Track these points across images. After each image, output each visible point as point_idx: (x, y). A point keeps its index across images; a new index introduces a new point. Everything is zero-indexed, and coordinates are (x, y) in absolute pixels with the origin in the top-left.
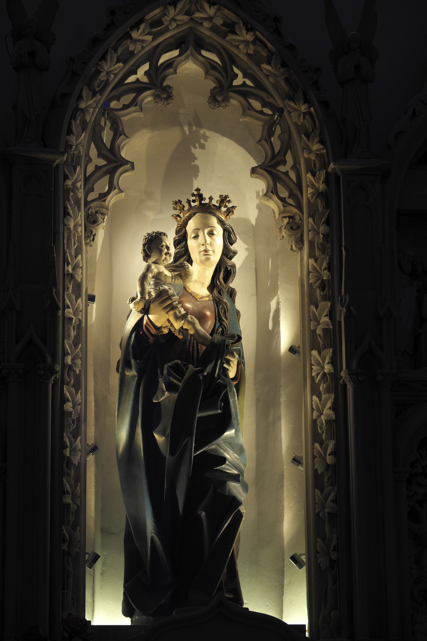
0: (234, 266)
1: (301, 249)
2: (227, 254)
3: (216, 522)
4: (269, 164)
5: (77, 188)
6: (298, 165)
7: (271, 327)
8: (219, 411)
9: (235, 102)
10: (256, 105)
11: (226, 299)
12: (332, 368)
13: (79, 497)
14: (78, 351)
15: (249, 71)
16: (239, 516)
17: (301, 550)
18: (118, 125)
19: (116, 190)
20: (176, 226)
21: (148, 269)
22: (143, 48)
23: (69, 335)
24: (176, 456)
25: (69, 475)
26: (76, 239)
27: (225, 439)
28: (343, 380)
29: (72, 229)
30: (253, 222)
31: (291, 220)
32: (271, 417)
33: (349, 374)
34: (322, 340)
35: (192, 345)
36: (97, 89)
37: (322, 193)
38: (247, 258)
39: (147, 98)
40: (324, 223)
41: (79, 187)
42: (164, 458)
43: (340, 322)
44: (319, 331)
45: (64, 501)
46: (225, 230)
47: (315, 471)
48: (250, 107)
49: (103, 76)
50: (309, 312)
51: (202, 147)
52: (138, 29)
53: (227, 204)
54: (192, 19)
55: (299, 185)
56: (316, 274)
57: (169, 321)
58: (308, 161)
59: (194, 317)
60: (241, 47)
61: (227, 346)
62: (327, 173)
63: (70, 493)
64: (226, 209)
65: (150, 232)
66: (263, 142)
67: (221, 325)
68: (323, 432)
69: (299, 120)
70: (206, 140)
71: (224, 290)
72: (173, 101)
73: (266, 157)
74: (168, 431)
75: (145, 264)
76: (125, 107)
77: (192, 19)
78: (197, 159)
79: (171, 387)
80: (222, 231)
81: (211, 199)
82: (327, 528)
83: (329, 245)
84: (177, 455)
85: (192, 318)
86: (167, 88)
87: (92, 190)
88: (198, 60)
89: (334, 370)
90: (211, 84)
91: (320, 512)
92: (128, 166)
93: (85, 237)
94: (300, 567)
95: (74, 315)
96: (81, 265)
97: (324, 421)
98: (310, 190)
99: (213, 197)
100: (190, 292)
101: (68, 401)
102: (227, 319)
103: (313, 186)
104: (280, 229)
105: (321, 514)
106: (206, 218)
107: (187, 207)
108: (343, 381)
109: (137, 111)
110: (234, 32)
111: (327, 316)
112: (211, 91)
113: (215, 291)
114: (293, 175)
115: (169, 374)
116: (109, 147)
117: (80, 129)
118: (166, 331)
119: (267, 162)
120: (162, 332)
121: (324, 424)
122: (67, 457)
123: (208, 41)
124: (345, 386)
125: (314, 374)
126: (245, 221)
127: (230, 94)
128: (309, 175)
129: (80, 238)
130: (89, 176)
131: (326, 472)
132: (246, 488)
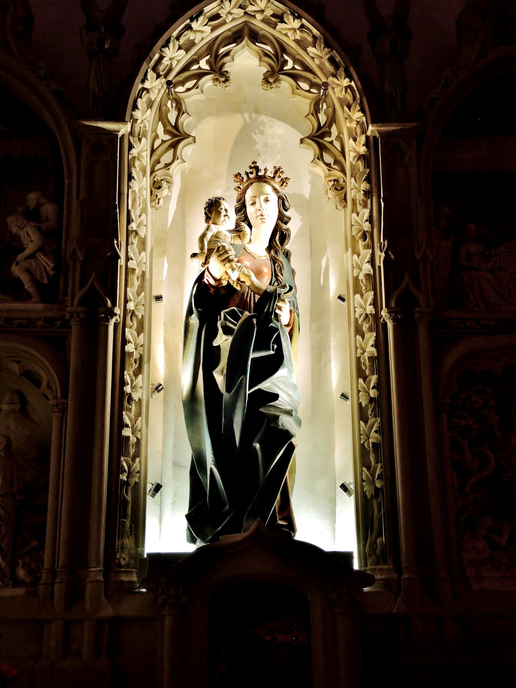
0: (288, 230)
1: (345, 207)
2: (282, 219)
3: (269, 453)
4: (317, 134)
5: (142, 157)
6: (341, 135)
7: (322, 283)
8: (272, 352)
9: (286, 83)
10: (305, 86)
11: (281, 258)
12: (373, 309)
13: (140, 430)
14: (141, 299)
15: (297, 57)
16: (291, 448)
17: (350, 480)
18: (181, 104)
19: (179, 160)
20: (237, 196)
21: (208, 229)
22: (203, 39)
23: (133, 284)
24: (232, 393)
25: (130, 410)
26: (141, 200)
27: (279, 378)
28: (384, 319)
29: (137, 192)
30: (307, 196)
31: (336, 182)
32: (323, 360)
33: (388, 312)
34: (364, 285)
35: (249, 295)
36: (161, 73)
37: (362, 155)
38: (302, 227)
39: (207, 81)
40: (364, 181)
41: (145, 156)
42: (221, 395)
43: (380, 267)
44: (361, 277)
45: (123, 434)
46: (279, 198)
47: (360, 404)
48: (299, 87)
49: (166, 61)
50: (352, 261)
51: (262, 133)
52: (197, 21)
53: (281, 175)
54: (246, 13)
55: (343, 153)
56: (358, 227)
57: (227, 273)
58: (350, 130)
59: (250, 271)
60: (290, 34)
61: (279, 295)
62: (367, 137)
63: (130, 426)
64: (280, 179)
65: (211, 198)
66: (311, 116)
67: (277, 280)
68: (366, 369)
69: (342, 94)
70: (264, 127)
71: (280, 251)
72: (230, 85)
73: (313, 130)
74: (225, 372)
75: (206, 225)
76: (188, 90)
77: (246, 13)
78: (257, 143)
79: (227, 331)
80: (277, 199)
81: (266, 170)
82: (372, 458)
83: (369, 201)
84: (233, 392)
85: (248, 272)
86: (225, 73)
87: (158, 162)
88: (253, 50)
89: (375, 311)
90: (264, 69)
91: (365, 442)
92: (190, 140)
93: (151, 201)
94: (350, 495)
95: (138, 267)
96: (145, 224)
97: (367, 358)
98: (353, 154)
99: (268, 168)
100: (249, 252)
101: (130, 342)
102: (282, 275)
103: (355, 151)
104: (327, 192)
105: (366, 444)
106: (262, 187)
107: (245, 179)
108: (384, 320)
109: (198, 94)
110: (283, 21)
111: (368, 262)
112: (264, 74)
113: (272, 252)
114: (337, 144)
115: (226, 319)
116: (174, 125)
117: (145, 106)
118: (225, 283)
119: (314, 133)
120: (222, 284)
121: (367, 361)
122: (127, 394)
123: (261, 32)
124: (385, 325)
125: (357, 316)
126: (300, 196)
127: (280, 76)
128: (351, 140)
129: (145, 201)
130: (156, 149)
131: (370, 405)
132: (299, 423)
